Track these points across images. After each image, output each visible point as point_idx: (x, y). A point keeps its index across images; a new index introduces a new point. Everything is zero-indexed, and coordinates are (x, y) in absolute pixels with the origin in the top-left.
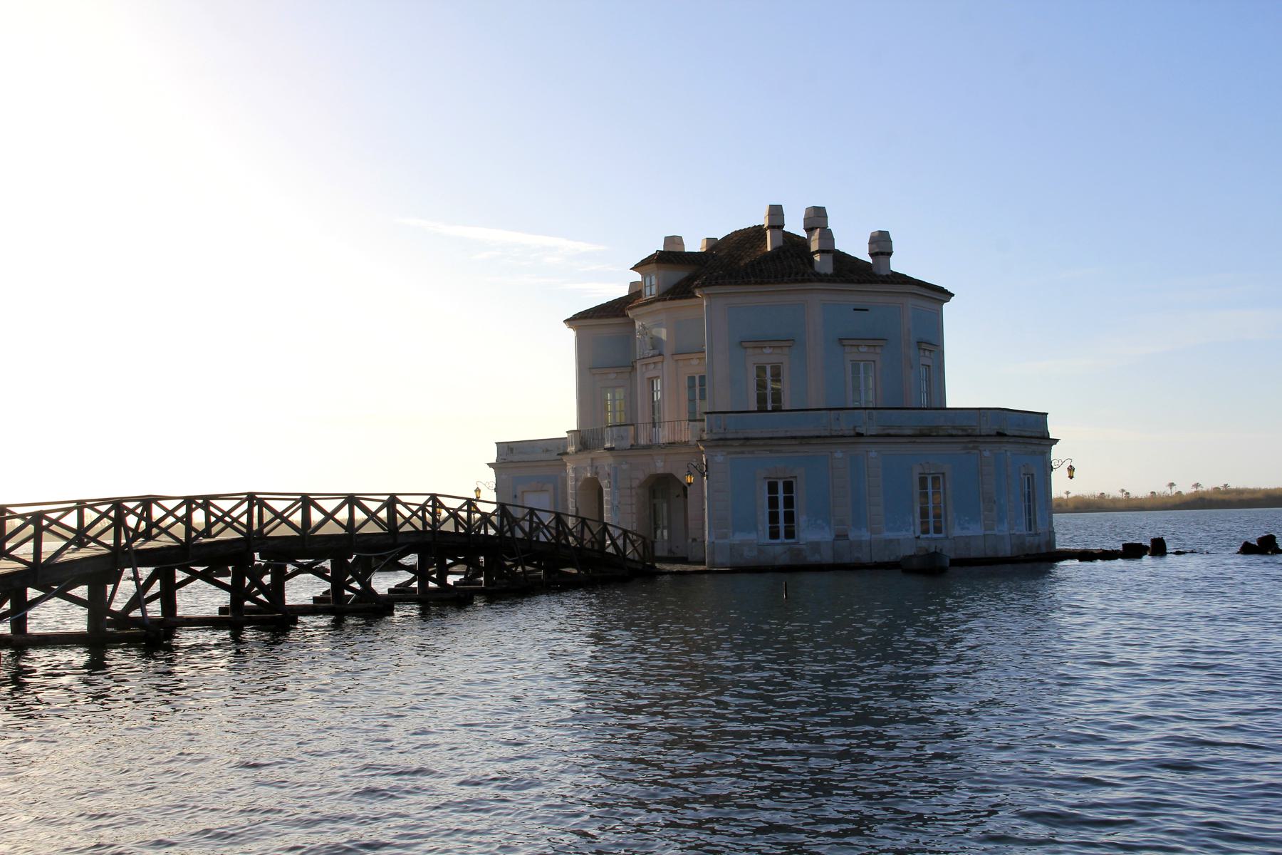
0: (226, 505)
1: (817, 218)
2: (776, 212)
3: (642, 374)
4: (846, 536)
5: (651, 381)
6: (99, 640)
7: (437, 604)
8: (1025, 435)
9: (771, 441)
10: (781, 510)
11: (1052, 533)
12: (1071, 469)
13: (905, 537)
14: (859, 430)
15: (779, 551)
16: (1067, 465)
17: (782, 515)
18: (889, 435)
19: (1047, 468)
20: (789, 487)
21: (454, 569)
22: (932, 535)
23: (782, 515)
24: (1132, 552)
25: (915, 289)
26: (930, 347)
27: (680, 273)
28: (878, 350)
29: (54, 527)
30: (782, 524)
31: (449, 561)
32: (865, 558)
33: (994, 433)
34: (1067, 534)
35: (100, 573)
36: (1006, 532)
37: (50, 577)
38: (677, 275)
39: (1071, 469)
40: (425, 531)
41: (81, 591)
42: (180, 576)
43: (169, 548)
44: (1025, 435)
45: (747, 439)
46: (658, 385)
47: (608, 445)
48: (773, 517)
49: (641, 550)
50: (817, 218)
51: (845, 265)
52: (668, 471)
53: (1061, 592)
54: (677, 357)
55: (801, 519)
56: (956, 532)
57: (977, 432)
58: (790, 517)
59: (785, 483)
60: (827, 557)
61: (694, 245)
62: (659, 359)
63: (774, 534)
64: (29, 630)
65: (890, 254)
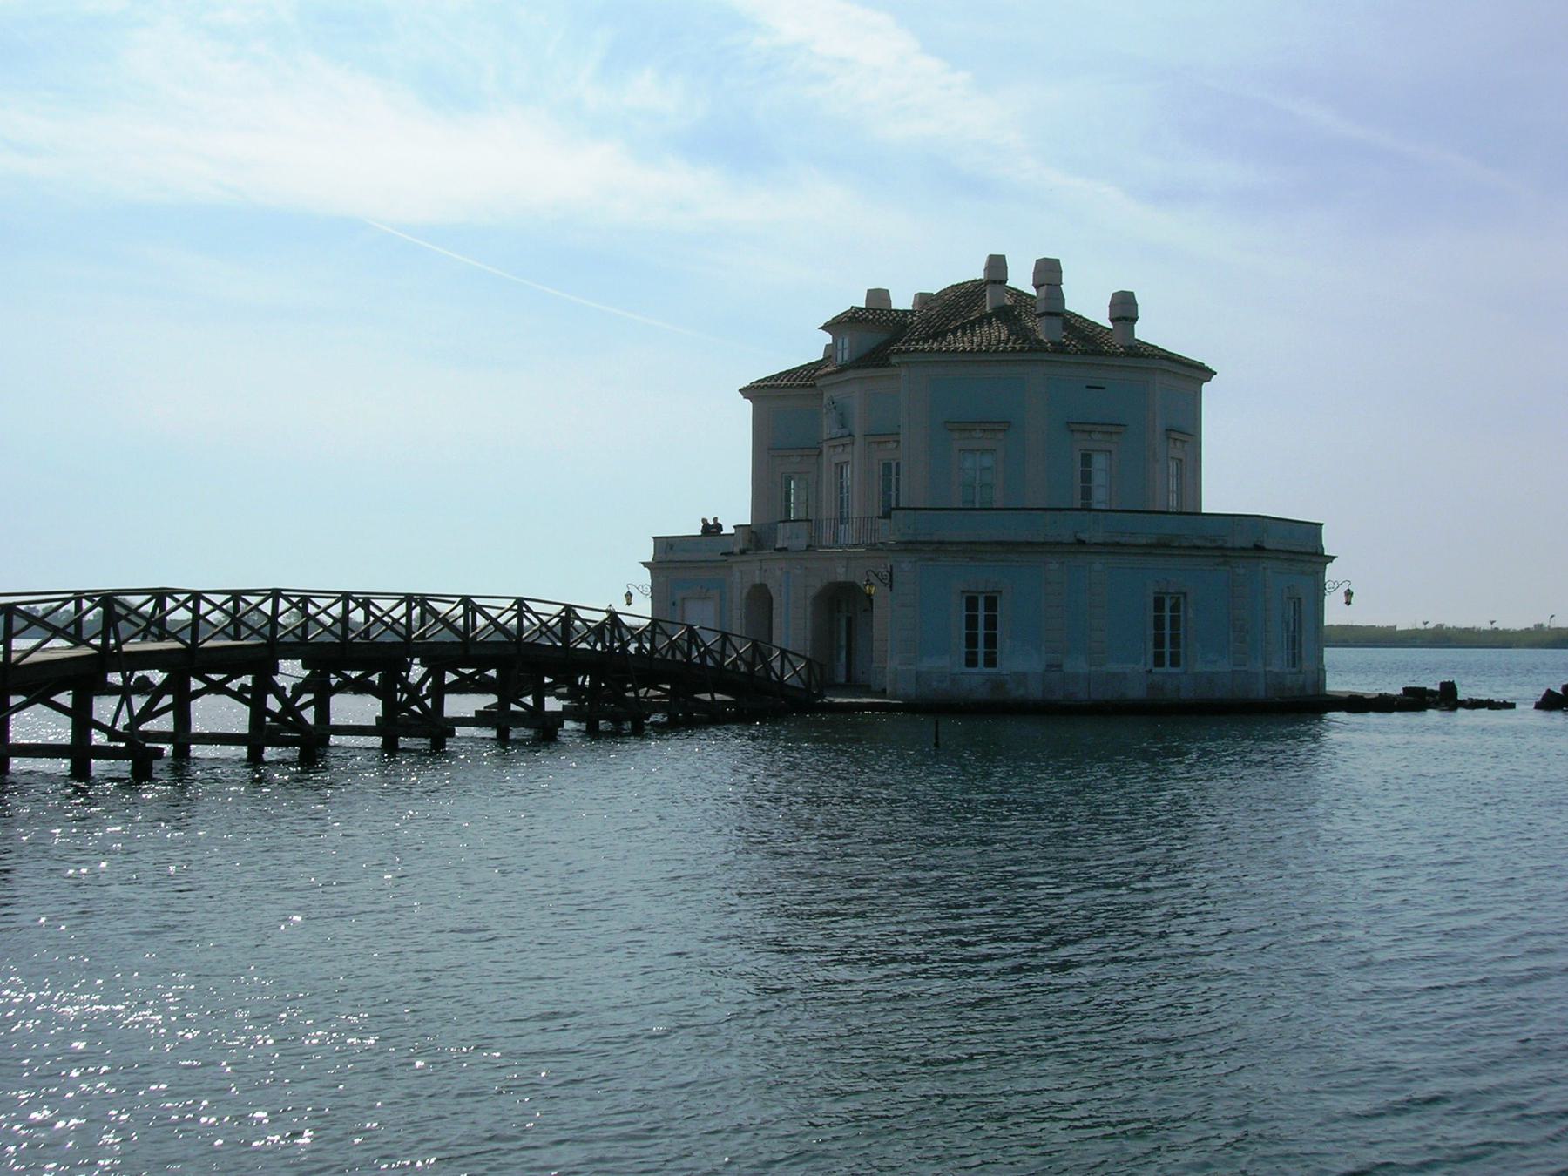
0: (386, 605)
1: (1048, 272)
2: (997, 265)
3: (830, 457)
4: (1059, 666)
5: (840, 467)
6: (388, 728)
7: (523, 732)
8: (1293, 551)
9: (971, 549)
10: (981, 632)
11: (1320, 672)
12: (1349, 594)
13: (1131, 670)
14: (1081, 536)
15: (975, 682)
16: (1344, 588)
17: (981, 637)
18: (1118, 544)
19: (1318, 591)
20: (991, 603)
21: (124, 714)
22: (1167, 668)
23: (981, 637)
24: (1415, 700)
25: (1166, 365)
26: (1185, 436)
27: (875, 337)
28: (1115, 438)
29: (132, 617)
30: (981, 649)
31: (547, 680)
32: (1082, 694)
33: (1251, 545)
34: (1344, 673)
35: (83, 679)
36: (1267, 668)
37: (39, 683)
38: (872, 339)
39: (1349, 594)
40: (510, 643)
41: (65, 698)
42: (195, 684)
43: (393, 643)
44: (1293, 551)
45: (941, 543)
46: (848, 472)
47: (779, 546)
48: (971, 640)
49: (803, 674)
50: (1048, 272)
51: (1078, 328)
52: (850, 578)
53: (1332, 737)
54: (871, 439)
55: (1004, 644)
56: (1200, 667)
57: (1229, 545)
58: (991, 641)
59: (987, 598)
60: (1035, 691)
61: (902, 301)
62: (847, 440)
63: (971, 661)
64: (193, 730)
65: (1135, 320)
